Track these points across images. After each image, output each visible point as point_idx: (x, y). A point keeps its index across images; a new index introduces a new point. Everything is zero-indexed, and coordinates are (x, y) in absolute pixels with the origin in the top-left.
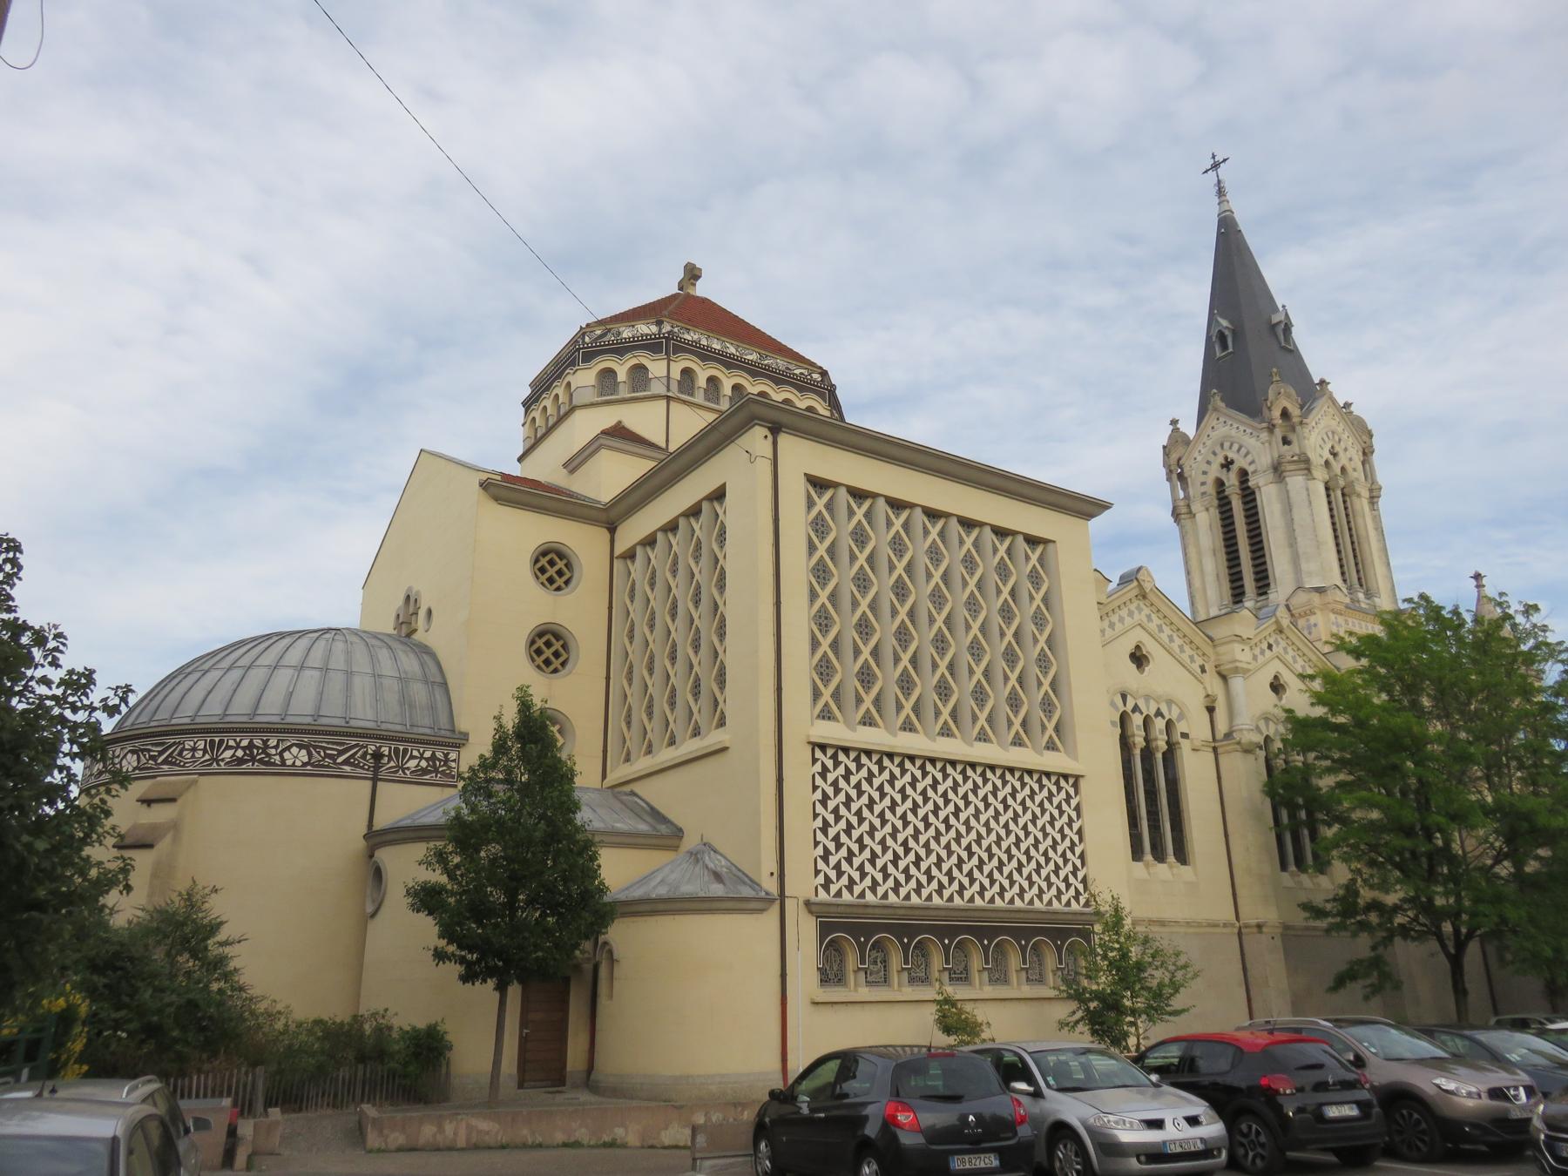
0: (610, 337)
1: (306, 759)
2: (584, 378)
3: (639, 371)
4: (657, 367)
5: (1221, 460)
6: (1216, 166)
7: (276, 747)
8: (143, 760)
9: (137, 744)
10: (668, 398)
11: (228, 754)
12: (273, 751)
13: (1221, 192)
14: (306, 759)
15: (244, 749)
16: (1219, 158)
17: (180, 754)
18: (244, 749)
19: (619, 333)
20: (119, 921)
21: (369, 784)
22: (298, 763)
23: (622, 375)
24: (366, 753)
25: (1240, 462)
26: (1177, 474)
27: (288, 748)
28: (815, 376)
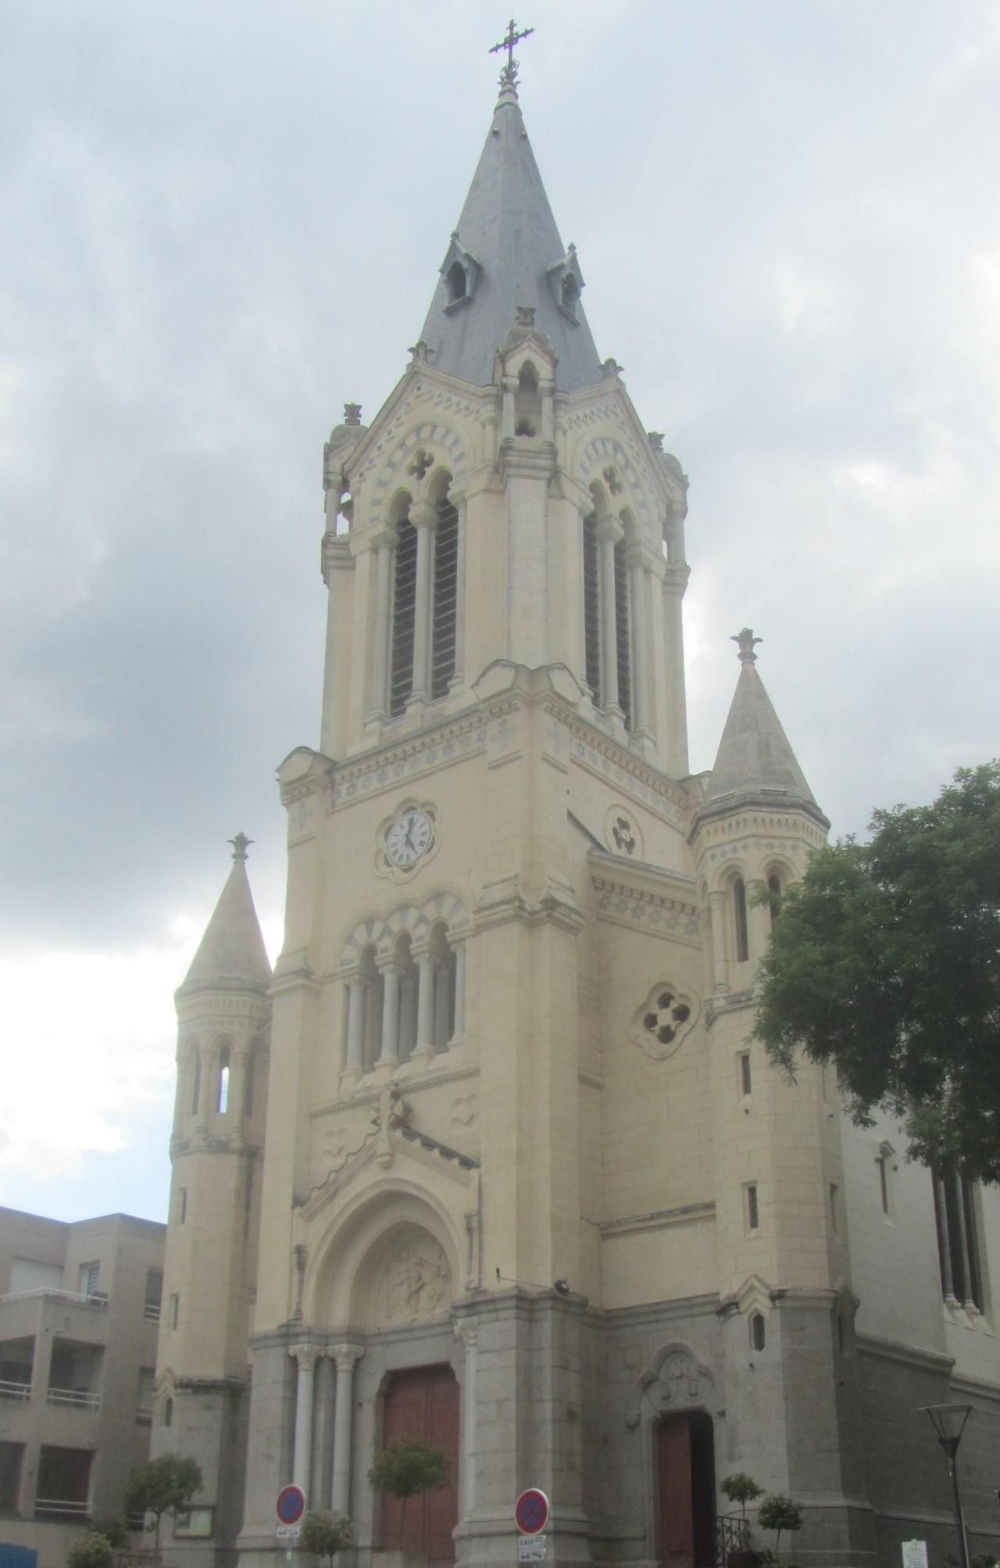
5: (412, 460)
6: (511, 42)
16: (519, 29)
20: (907, 1547)
25: (442, 459)
26: (338, 482)
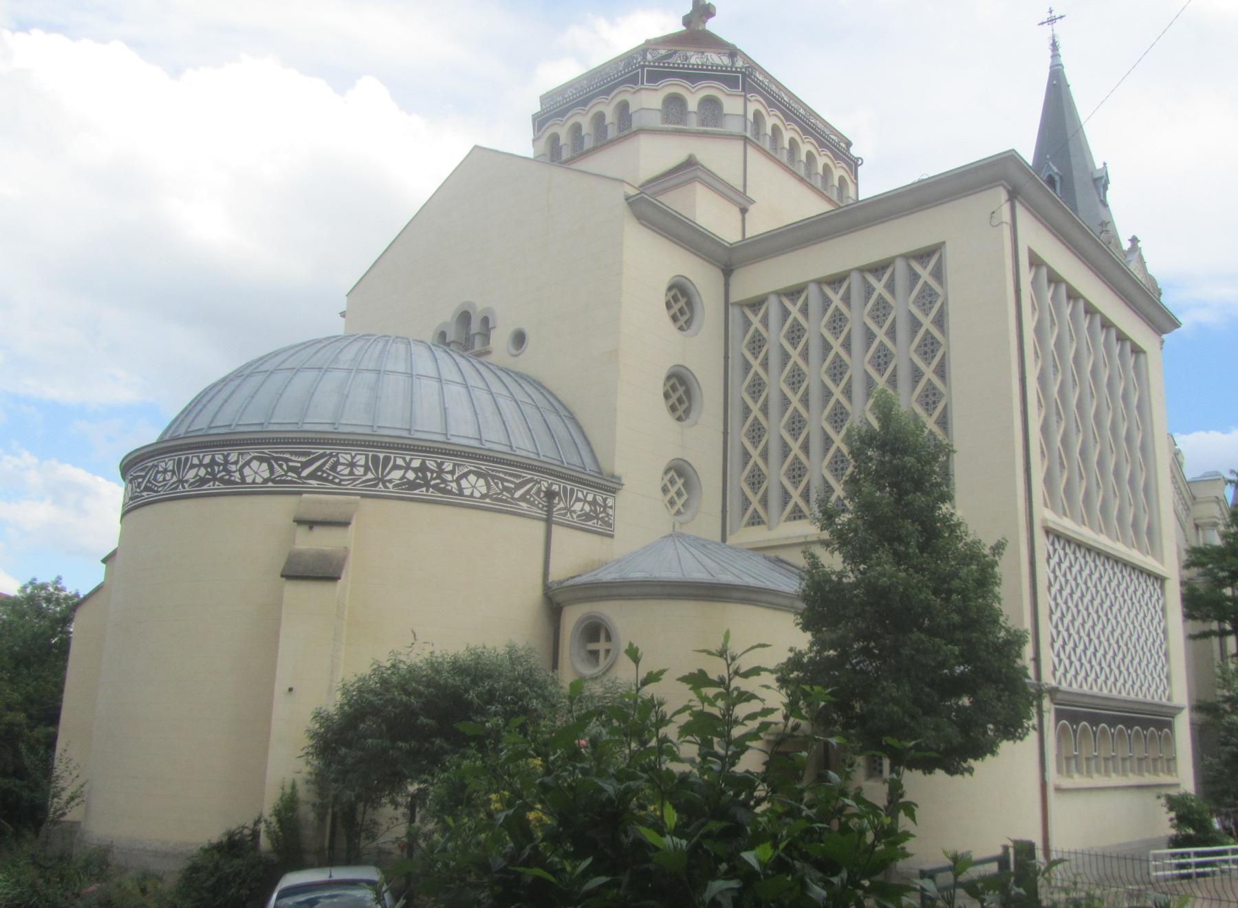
0: (677, 60)
1: (266, 475)
2: (649, 100)
3: (710, 103)
4: (732, 104)
6: (1052, 21)
7: (452, 472)
8: (279, 471)
9: (484, 467)
10: (745, 139)
11: (397, 475)
12: (449, 477)
13: (1054, 46)
14: (484, 490)
15: (415, 470)
16: (1056, 14)
17: (333, 468)
18: (415, 470)
19: (687, 58)
21: (541, 526)
22: (477, 494)
23: (693, 103)
24: (539, 490)
27: (465, 475)
28: (843, 145)
